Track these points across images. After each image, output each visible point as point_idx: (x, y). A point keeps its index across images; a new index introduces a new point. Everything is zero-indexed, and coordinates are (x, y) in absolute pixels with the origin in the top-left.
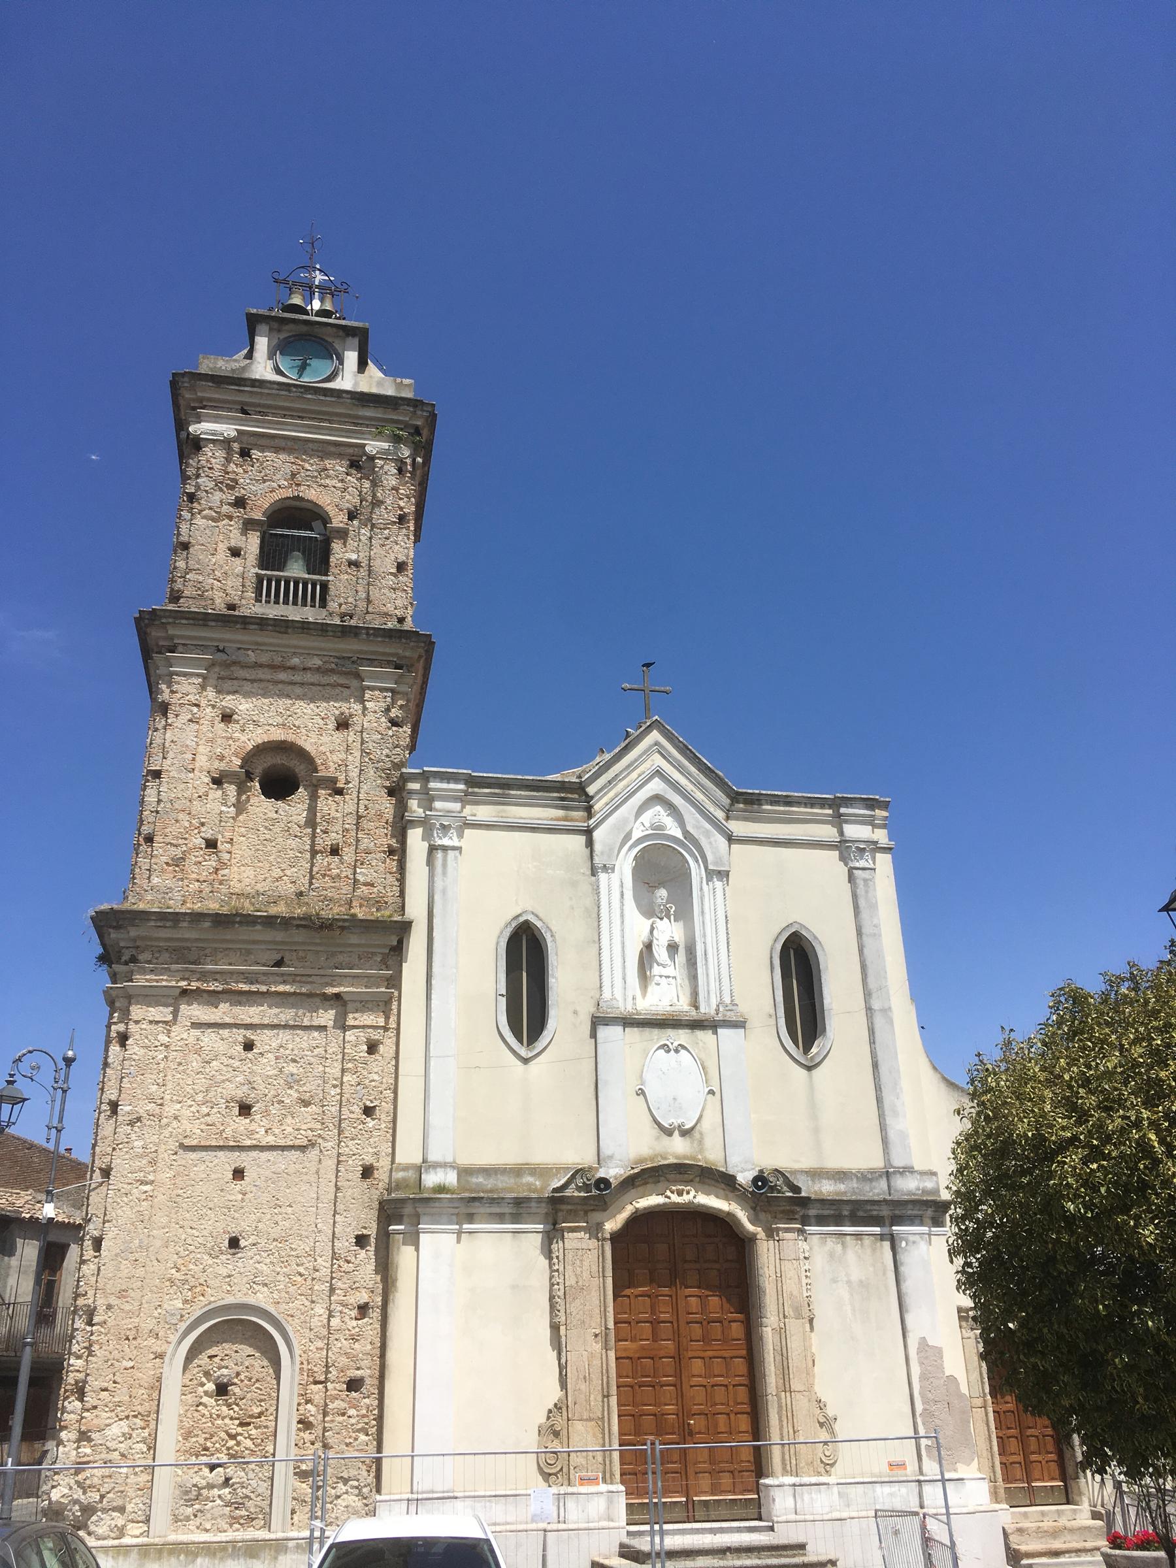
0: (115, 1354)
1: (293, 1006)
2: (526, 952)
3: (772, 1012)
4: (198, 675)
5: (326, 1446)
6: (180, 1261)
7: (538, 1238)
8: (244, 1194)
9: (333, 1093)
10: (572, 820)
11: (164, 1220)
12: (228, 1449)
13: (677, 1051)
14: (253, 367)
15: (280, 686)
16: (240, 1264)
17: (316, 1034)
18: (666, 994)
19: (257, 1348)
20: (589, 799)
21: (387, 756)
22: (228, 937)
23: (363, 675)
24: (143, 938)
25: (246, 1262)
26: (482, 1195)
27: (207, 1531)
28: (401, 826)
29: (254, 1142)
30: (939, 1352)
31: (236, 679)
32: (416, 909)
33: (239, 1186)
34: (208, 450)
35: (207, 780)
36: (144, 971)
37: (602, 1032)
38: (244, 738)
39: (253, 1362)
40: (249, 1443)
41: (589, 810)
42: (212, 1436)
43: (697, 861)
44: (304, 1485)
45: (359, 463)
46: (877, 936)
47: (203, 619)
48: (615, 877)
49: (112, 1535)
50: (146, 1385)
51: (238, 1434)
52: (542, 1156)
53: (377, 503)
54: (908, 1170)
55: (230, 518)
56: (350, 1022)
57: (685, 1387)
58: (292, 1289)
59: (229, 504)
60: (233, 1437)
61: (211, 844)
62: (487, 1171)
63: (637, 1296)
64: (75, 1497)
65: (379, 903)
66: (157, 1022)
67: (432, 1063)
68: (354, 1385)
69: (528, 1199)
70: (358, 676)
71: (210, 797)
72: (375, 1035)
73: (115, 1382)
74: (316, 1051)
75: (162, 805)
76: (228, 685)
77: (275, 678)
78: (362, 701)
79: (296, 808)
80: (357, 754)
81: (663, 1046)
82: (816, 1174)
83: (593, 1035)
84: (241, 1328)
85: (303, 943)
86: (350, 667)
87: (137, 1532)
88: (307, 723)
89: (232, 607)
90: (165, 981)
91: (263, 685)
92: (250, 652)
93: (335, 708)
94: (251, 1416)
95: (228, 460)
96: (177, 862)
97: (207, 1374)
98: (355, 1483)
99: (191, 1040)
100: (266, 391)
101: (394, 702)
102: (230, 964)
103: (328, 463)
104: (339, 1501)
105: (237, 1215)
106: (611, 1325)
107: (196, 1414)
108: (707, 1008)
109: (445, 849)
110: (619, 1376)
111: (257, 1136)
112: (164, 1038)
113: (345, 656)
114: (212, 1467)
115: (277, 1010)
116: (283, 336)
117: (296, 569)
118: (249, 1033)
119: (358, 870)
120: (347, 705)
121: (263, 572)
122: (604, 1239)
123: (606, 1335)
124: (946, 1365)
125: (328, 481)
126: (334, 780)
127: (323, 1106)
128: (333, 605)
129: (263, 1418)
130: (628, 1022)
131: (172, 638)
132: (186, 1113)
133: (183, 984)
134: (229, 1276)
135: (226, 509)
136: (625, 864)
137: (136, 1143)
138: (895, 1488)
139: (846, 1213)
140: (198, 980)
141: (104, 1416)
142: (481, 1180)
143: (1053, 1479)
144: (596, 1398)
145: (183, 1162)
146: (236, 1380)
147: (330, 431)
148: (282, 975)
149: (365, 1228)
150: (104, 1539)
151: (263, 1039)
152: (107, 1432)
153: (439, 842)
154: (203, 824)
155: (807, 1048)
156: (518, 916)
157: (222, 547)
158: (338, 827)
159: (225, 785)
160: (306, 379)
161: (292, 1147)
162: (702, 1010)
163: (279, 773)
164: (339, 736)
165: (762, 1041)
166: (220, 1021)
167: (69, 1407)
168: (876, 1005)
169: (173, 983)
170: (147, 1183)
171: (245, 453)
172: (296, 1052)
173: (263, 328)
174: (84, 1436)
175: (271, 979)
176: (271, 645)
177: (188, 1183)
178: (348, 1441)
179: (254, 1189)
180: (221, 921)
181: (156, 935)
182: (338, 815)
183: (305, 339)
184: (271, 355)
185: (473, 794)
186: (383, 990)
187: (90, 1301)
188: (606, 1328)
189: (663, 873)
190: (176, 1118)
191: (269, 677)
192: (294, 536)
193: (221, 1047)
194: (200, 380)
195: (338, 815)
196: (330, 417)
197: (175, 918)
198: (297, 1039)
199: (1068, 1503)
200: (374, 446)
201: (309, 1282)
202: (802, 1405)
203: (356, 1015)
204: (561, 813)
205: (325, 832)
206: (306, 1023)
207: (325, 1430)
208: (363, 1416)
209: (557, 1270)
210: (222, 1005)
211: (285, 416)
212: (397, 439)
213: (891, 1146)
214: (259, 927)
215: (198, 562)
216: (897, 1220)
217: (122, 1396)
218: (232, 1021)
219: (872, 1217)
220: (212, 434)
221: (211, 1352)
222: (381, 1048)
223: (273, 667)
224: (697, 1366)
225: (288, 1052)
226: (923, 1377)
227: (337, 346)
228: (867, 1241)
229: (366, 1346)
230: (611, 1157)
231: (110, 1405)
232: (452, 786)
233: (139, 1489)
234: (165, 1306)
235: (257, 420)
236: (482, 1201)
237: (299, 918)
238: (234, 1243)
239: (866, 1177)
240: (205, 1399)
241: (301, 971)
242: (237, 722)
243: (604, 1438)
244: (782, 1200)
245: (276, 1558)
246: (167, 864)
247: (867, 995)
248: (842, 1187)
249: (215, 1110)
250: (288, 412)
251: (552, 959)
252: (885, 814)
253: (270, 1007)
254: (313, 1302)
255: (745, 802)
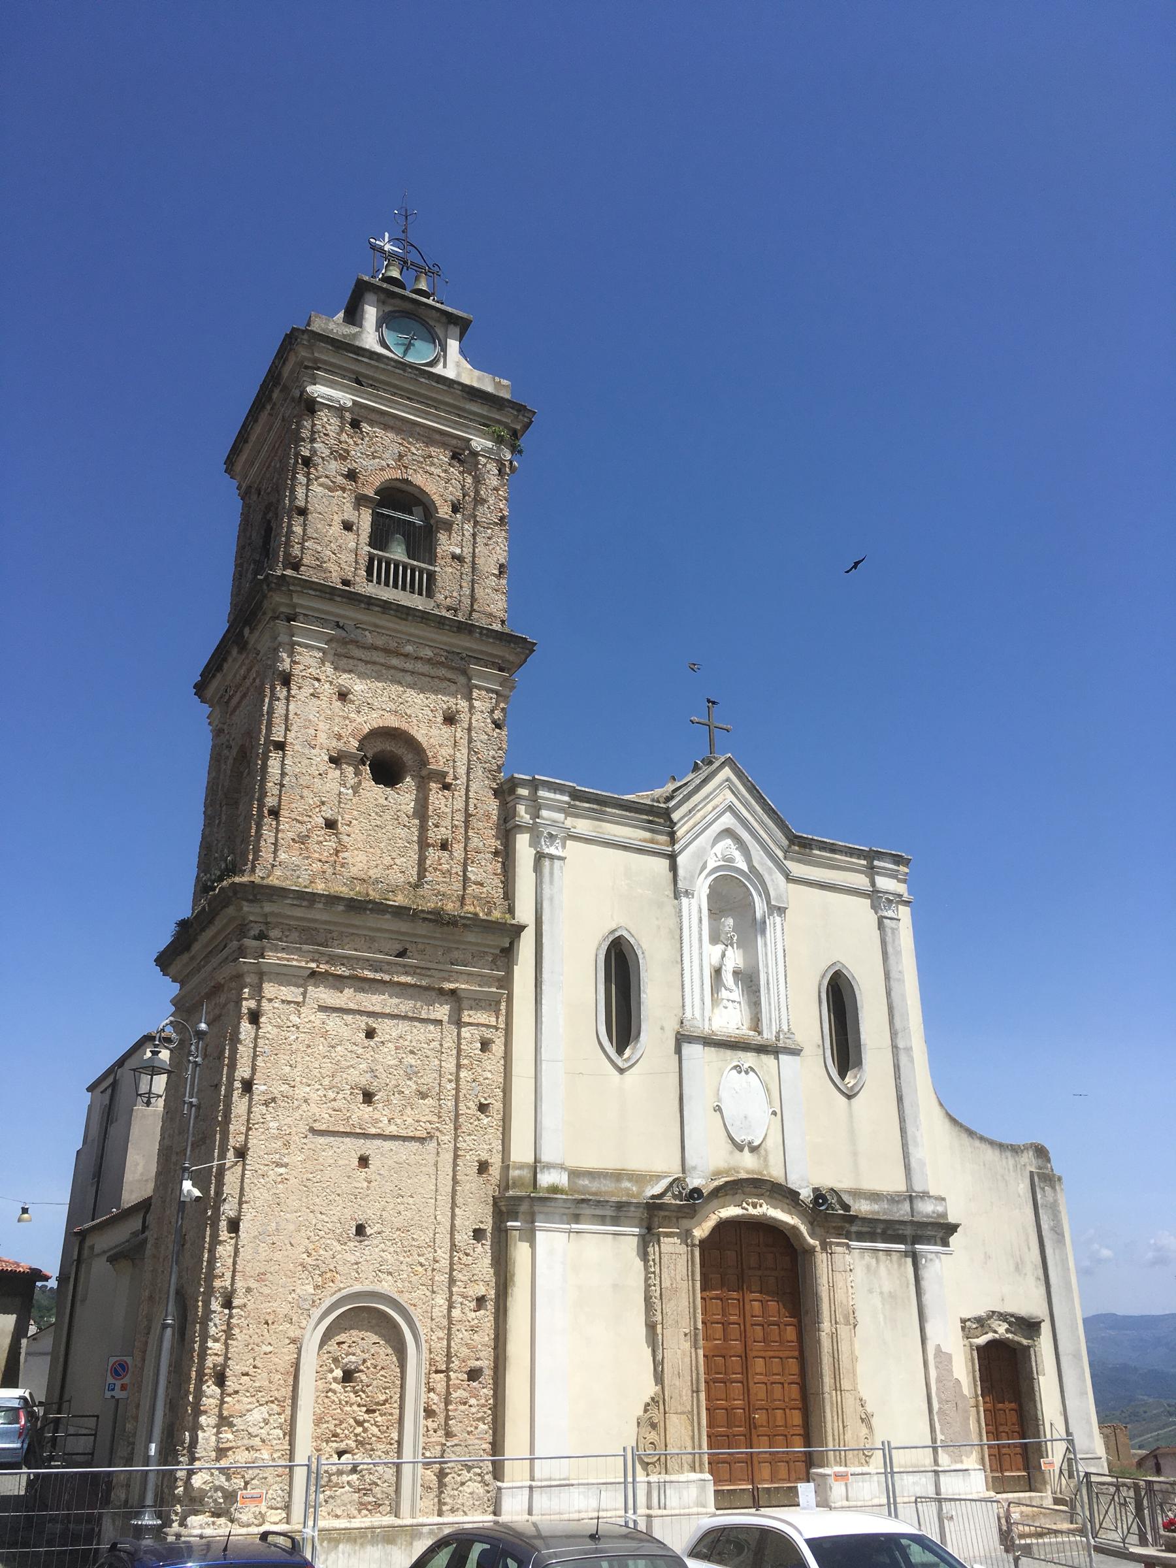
0: (256, 1338)
1: (411, 998)
2: (620, 965)
3: (820, 1042)
4: (319, 649)
5: (449, 1435)
6: (311, 1246)
7: (634, 1241)
8: (370, 1182)
9: (449, 1087)
10: (657, 843)
11: (296, 1204)
12: (356, 1435)
13: (747, 1072)
14: (364, 336)
15: (392, 671)
16: (366, 1252)
17: (432, 1027)
18: (730, 1018)
19: (382, 1336)
20: (673, 824)
21: (494, 758)
22: (357, 923)
23: (471, 673)
24: (272, 914)
25: (373, 1250)
26: (588, 1197)
27: (337, 1516)
28: (507, 830)
29: (379, 1131)
30: (949, 1356)
31: (352, 658)
32: (524, 913)
33: (362, 1174)
34: (323, 415)
35: (326, 758)
36: (276, 949)
37: (687, 1049)
38: (360, 719)
39: (378, 1349)
40: (375, 1430)
41: (672, 835)
42: (341, 1422)
43: (760, 896)
44: (428, 1472)
45: (462, 455)
46: (901, 981)
47: (327, 592)
48: (694, 901)
49: (256, 1522)
50: (282, 1370)
51: (364, 1421)
52: (636, 1163)
53: (479, 501)
54: (925, 1195)
55: (344, 490)
56: (465, 1019)
57: (751, 1384)
58: (414, 1279)
59: (342, 475)
60: (360, 1423)
61: (331, 824)
62: (592, 1175)
63: (711, 1299)
64: (217, 1483)
65: (489, 903)
66: (289, 1002)
67: (544, 1066)
68: (474, 1375)
69: (629, 1204)
70: (464, 672)
71: (329, 776)
72: (488, 1034)
73: (255, 1367)
74: (433, 1044)
75: (287, 778)
76: (343, 662)
77: (387, 662)
78: (469, 698)
79: (404, 797)
80: (465, 751)
81: (735, 1067)
82: (857, 1194)
83: (678, 1051)
84: (368, 1315)
85: (425, 936)
86: (457, 663)
87: (277, 1519)
88: (417, 712)
89: (346, 582)
90: (296, 961)
91: (377, 668)
92: (367, 633)
93: (444, 702)
94: (378, 1404)
95: (342, 429)
96: (302, 839)
97: (336, 1360)
98: (478, 1471)
99: (318, 1023)
100: (382, 366)
101: (497, 703)
102: (356, 950)
103: (433, 451)
104: (465, 1488)
105: (363, 1203)
106: (700, 1326)
107: (326, 1400)
108: (768, 1035)
109: (552, 857)
110: (707, 1373)
111: (380, 1125)
112: (294, 1019)
113: (462, 652)
114: (340, 1454)
115: (397, 1001)
116: (388, 309)
117: (398, 553)
118: (370, 1021)
119: (470, 869)
120: (454, 700)
121: (375, 552)
122: (693, 1245)
123: (696, 1335)
124: (954, 1369)
125: (433, 469)
126: (444, 775)
127: (440, 1099)
128: (440, 597)
129: (387, 1406)
130: (709, 1041)
131: (294, 606)
132: (314, 1096)
133: (313, 965)
134: (357, 1263)
135: (340, 480)
136: (702, 888)
137: (271, 1124)
138: (917, 1477)
139: (879, 1231)
140: (327, 963)
141: (246, 1401)
142: (587, 1182)
143: (1018, 1470)
144: (686, 1392)
145: (312, 1146)
146: (362, 1367)
147: (437, 419)
148: (405, 966)
149: (482, 1222)
150: (249, 1525)
151: (386, 1029)
152: (248, 1417)
153: (546, 851)
154: (323, 803)
155: (620, 1051)
156: (615, 930)
157: (337, 519)
158: (447, 822)
159: (344, 766)
160: (410, 359)
161: (413, 1138)
162: (765, 1036)
163: (388, 759)
164: (447, 731)
165: (809, 1069)
166: (345, 1006)
167: (209, 1392)
168: (901, 1045)
169: (303, 964)
170: (282, 1166)
171: (355, 424)
172: (414, 1044)
173: (370, 297)
174: (224, 1421)
175: (394, 969)
176: (388, 629)
177: (318, 1167)
178: (469, 1429)
179: (378, 1177)
180: (355, 906)
181: (289, 913)
182: (448, 810)
183: (407, 314)
184: (379, 327)
185: (574, 807)
186: (494, 990)
187: (228, 1283)
188: (696, 1329)
189: (733, 903)
190: (306, 1101)
191: (383, 661)
192: (401, 516)
193: (346, 1032)
194: (321, 341)
195: (448, 810)
196: (437, 404)
197: (309, 899)
198: (415, 1031)
199: (1030, 1491)
200: (479, 443)
201: (429, 1273)
202: (850, 1402)
203: (471, 1012)
204: (648, 835)
205: (437, 826)
206: (424, 1016)
207: (447, 1418)
208: (483, 1406)
209: (654, 1273)
210: (346, 990)
211: (394, 394)
212: (499, 440)
213: (912, 1172)
214: (388, 916)
215: (316, 531)
216: (917, 1239)
217: (261, 1380)
218: (356, 1007)
219: (898, 1235)
220: (328, 400)
221: (339, 1338)
222: (494, 1047)
223: (387, 651)
224: (759, 1365)
225: (406, 1043)
226: (939, 1380)
227: (440, 331)
228: (895, 1256)
229: (485, 1336)
230: (694, 1168)
231: (251, 1390)
232: (558, 797)
233: (278, 1476)
234: (298, 1291)
235: (371, 394)
236: (593, 1202)
237: (429, 913)
238: (360, 1230)
239: (894, 1199)
240: (334, 1386)
241: (422, 964)
242: (352, 702)
243: (693, 1431)
244: (832, 1214)
245: (411, 1544)
246: (293, 840)
247: (894, 1034)
248: (876, 1207)
249: (340, 1096)
250: (397, 391)
251: (857, 992)
252: (907, 870)
253: (391, 996)
254: (433, 1292)
255: (800, 845)
